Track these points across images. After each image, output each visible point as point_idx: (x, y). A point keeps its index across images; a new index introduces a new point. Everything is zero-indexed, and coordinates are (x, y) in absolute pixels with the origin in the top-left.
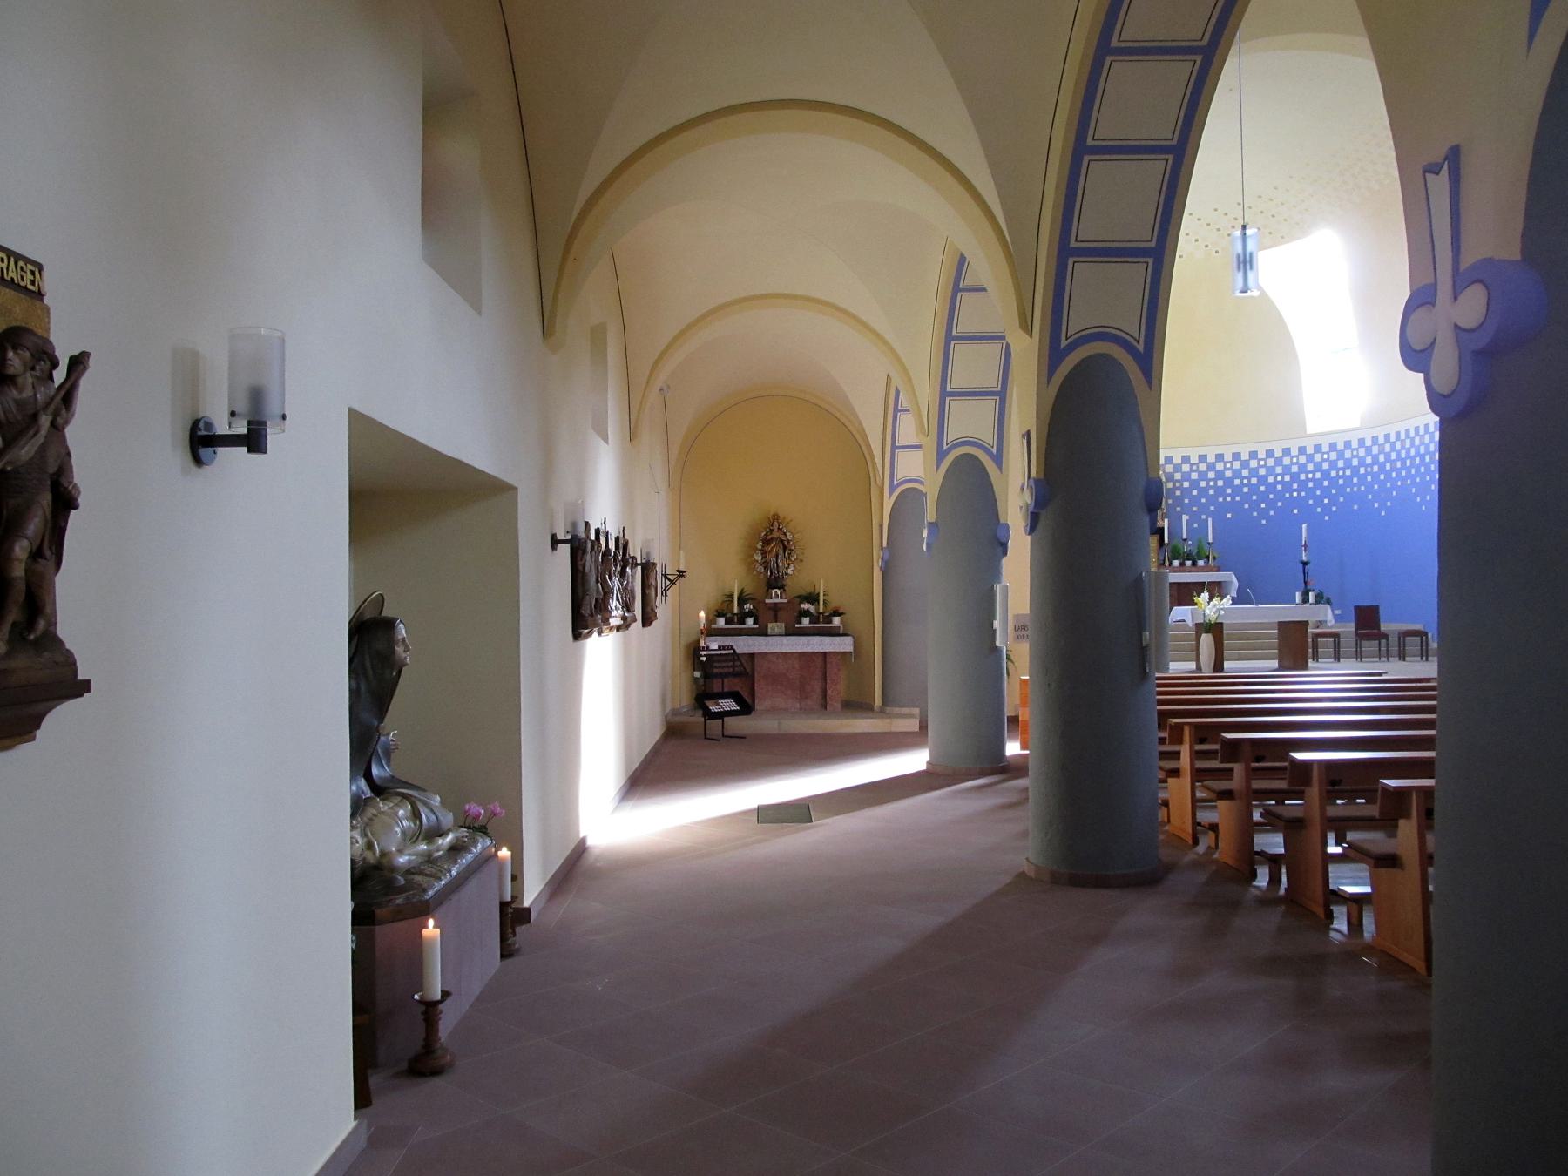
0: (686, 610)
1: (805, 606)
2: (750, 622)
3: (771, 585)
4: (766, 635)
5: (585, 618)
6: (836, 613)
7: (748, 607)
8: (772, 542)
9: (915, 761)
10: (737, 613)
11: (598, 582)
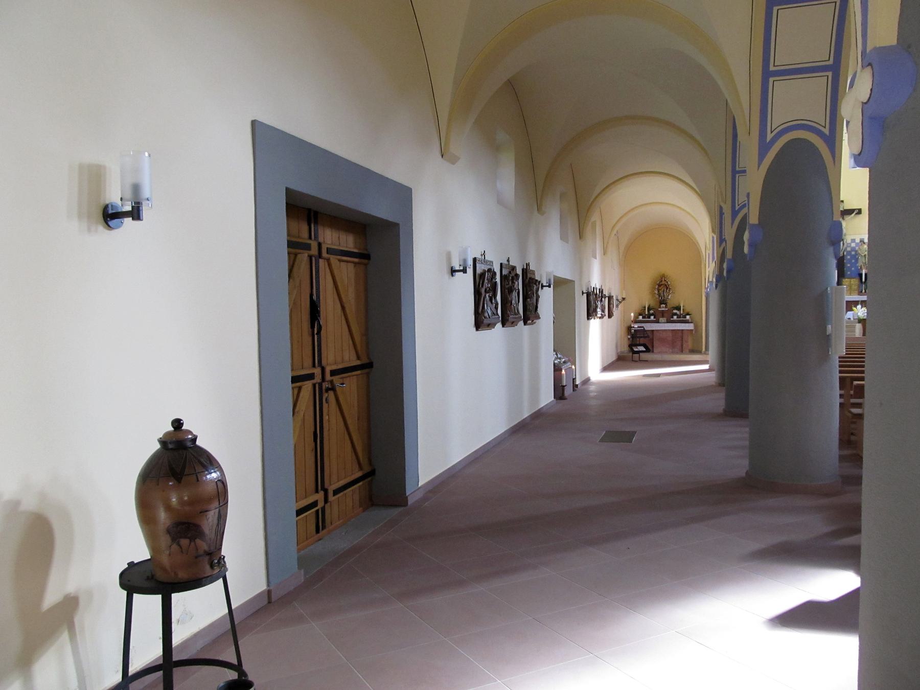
0: (626, 313)
1: (675, 311)
2: (652, 317)
3: (662, 303)
4: (658, 322)
5: (591, 313)
6: (688, 314)
7: (652, 312)
8: (662, 285)
9: (706, 367)
10: (647, 314)
11: (595, 302)
